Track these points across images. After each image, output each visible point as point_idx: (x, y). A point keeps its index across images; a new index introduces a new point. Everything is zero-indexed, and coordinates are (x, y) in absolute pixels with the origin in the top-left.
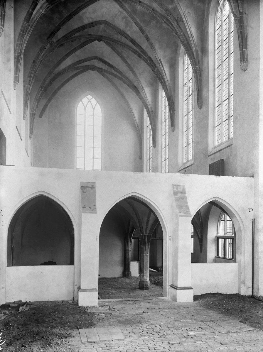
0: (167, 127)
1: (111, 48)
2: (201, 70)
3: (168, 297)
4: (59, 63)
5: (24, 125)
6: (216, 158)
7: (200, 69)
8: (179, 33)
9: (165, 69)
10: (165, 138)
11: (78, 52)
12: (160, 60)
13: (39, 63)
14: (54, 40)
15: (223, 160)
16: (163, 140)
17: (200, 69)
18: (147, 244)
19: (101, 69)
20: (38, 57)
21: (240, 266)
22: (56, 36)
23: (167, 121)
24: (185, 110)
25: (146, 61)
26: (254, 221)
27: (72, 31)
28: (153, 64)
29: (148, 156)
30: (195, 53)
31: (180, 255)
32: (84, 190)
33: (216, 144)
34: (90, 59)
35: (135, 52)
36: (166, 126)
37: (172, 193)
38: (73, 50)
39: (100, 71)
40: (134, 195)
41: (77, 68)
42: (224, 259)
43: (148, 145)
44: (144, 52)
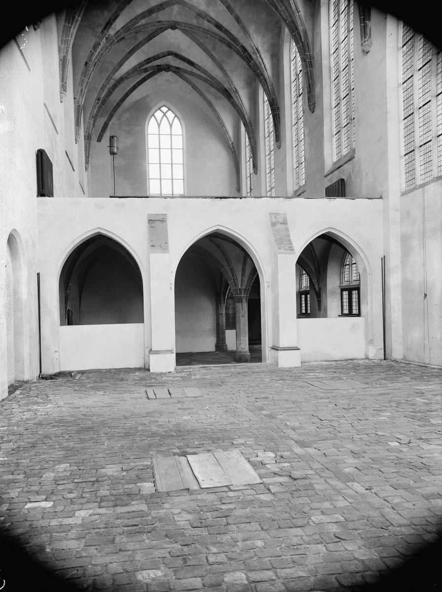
0: (272, 143)
1: (191, 38)
2: (311, 58)
3: (269, 361)
4: (121, 64)
5: (77, 151)
6: (335, 178)
7: (310, 56)
8: (279, 7)
9: (265, 61)
10: (270, 159)
11: (145, 47)
12: (256, 49)
13: (93, 66)
14: (112, 32)
15: (342, 180)
16: (267, 162)
17: (310, 56)
18: (244, 301)
19: (178, 68)
20: (91, 58)
21: (367, 321)
22: (113, 26)
23: (272, 134)
24: (294, 117)
25: (238, 53)
26: (383, 260)
27: (135, 18)
28: (248, 56)
29: (249, 186)
30: (302, 35)
31: (280, 305)
32: (153, 225)
33: (335, 160)
34: (164, 55)
35: (222, 40)
36: (270, 143)
37: (269, 224)
38: (138, 44)
39: (177, 71)
40: (218, 229)
41: (146, 70)
42: (350, 314)
43: (248, 171)
44: (235, 40)
